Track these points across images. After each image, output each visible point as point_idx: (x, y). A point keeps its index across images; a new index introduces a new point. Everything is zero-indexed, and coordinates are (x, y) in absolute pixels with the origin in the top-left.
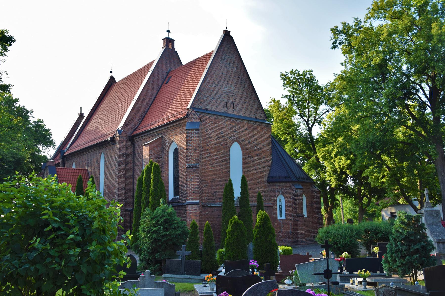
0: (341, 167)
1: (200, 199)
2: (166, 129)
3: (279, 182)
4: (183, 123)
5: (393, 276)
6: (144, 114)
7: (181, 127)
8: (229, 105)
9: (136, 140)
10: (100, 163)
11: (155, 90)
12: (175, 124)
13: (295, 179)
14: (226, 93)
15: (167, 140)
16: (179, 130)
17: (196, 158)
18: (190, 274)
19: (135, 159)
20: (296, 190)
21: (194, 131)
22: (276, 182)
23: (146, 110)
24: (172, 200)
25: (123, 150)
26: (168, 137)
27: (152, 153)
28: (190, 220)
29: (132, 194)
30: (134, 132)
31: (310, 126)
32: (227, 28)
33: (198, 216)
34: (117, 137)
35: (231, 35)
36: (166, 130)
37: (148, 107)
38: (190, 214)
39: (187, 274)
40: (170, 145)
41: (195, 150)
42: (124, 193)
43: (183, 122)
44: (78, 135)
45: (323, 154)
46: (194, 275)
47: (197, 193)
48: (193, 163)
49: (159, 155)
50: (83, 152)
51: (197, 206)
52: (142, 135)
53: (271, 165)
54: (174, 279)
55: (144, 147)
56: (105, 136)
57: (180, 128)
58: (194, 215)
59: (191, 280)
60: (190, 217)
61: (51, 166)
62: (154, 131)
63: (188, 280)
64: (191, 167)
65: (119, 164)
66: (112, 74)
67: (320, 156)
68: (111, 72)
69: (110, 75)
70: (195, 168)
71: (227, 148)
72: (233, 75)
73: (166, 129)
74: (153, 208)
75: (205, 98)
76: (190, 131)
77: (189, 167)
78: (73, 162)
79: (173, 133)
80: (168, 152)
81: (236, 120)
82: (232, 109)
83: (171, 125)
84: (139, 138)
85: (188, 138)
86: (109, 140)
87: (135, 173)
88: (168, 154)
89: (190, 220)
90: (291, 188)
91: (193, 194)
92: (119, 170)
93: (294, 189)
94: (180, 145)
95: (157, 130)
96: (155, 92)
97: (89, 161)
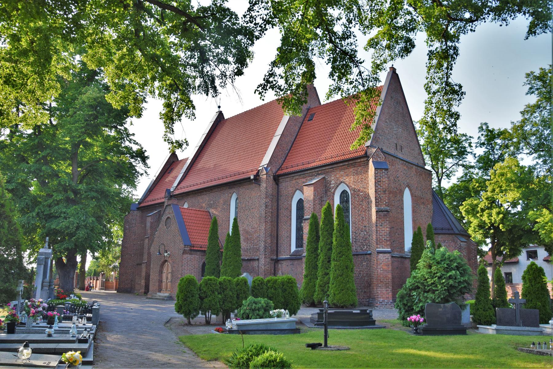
0: (493, 222)
1: (391, 246)
2: (331, 168)
3: (442, 234)
4: (359, 162)
5: (78, 353)
6: (287, 152)
7: (355, 167)
8: (398, 147)
9: (281, 180)
10: (230, 204)
11: (297, 127)
12: (346, 163)
13: (457, 232)
14: (395, 134)
15: (333, 181)
16: (351, 170)
17: (385, 201)
18: (528, 326)
19: (280, 202)
20: (462, 243)
21: (383, 171)
22: (439, 234)
23: (289, 149)
24: (295, 251)
25: (270, 190)
26: (332, 179)
27: (316, 195)
28: (381, 271)
29: (275, 241)
30: (279, 172)
31: (440, 178)
32: (393, 65)
33: (390, 266)
34: (263, 175)
35: (397, 72)
36: (332, 169)
37: (290, 145)
38: (381, 263)
39: (525, 325)
40: (338, 186)
41: (385, 191)
42: (270, 240)
43: (359, 161)
44: (186, 173)
45: (466, 207)
46: (532, 327)
47: (389, 241)
48: (383, 207)
49: (321, 197)
50: (202, 192)
51: (389, 255)
52: (293, 175)
53: (433, 215)
54: (509, 332)
55: (304, 187)
56: (239, 174)
57: (353, 168)
58: (386, 265)
59: (529, 333)
60: (382, 267)
61: (174, 204)
62: (309, 172)
63: (525, 333)
64: (381, 211)
65: (266, 206)
66: (221, 109)
67: (462, 209)
68: (219, 107)
69: (217, 110)
70: (386, 213)
71: (402, 193)
72: (400, 115)
73: (331, 168)
74: (339, 255)
75: (380, 137)
76: (379, 170)
77: (380, 211)
78: (184, 203)
79: (342, 173)
80: (334, 194)
81: (407, 164)
82: (400, 151)
83: (341, 164)
84: (287, 178)
85: (377, 178)
86: (252, 177)
87: (280, 217)
88: (333, 197)
89: (381, 271)
90: (453, 241)
91: (383, 241)
92: (266, 213)
93: (459, 242)
94: (353, 187)
95: (317, 170)
96: (297, 129)
97: (212, 202)
